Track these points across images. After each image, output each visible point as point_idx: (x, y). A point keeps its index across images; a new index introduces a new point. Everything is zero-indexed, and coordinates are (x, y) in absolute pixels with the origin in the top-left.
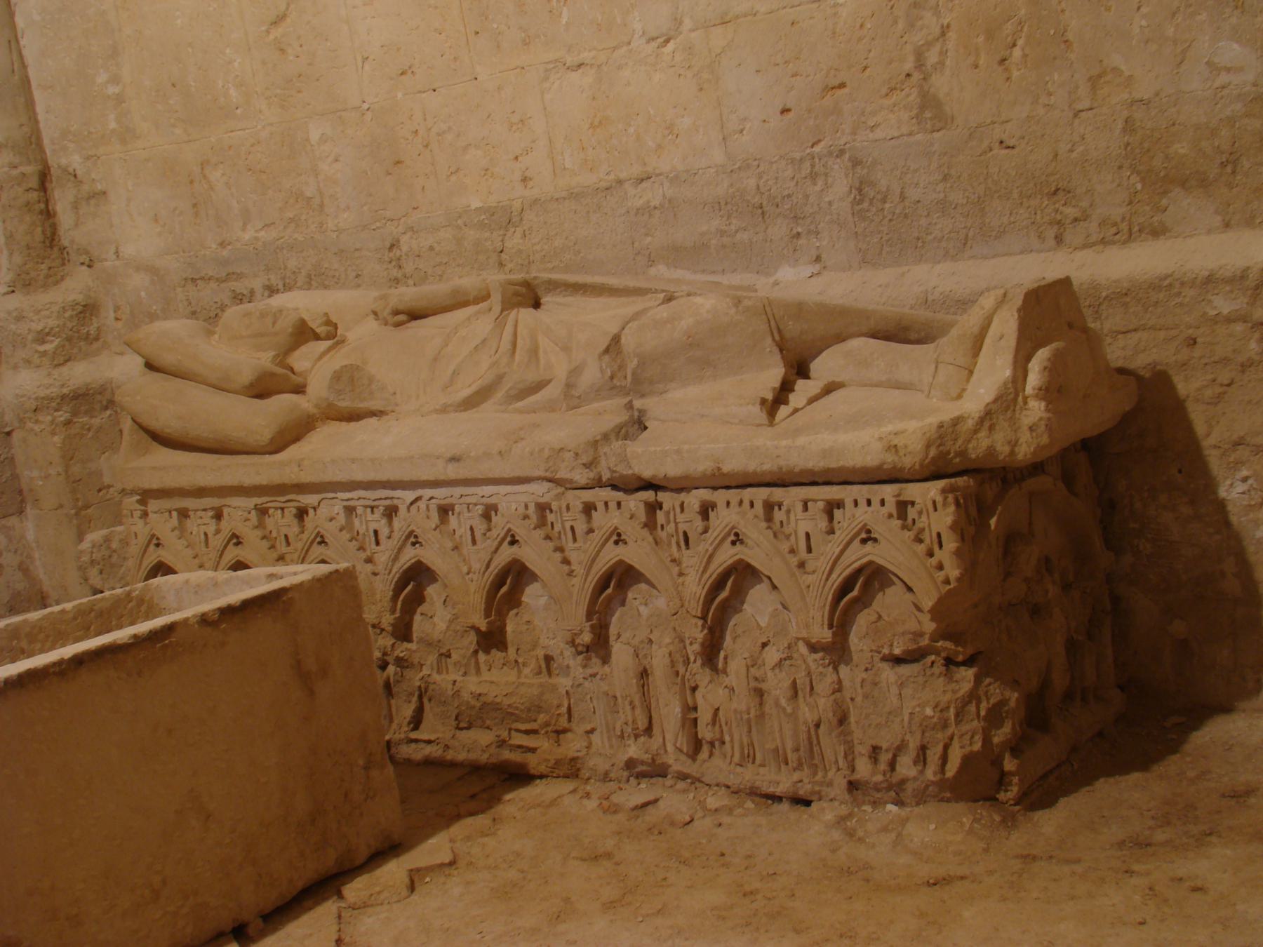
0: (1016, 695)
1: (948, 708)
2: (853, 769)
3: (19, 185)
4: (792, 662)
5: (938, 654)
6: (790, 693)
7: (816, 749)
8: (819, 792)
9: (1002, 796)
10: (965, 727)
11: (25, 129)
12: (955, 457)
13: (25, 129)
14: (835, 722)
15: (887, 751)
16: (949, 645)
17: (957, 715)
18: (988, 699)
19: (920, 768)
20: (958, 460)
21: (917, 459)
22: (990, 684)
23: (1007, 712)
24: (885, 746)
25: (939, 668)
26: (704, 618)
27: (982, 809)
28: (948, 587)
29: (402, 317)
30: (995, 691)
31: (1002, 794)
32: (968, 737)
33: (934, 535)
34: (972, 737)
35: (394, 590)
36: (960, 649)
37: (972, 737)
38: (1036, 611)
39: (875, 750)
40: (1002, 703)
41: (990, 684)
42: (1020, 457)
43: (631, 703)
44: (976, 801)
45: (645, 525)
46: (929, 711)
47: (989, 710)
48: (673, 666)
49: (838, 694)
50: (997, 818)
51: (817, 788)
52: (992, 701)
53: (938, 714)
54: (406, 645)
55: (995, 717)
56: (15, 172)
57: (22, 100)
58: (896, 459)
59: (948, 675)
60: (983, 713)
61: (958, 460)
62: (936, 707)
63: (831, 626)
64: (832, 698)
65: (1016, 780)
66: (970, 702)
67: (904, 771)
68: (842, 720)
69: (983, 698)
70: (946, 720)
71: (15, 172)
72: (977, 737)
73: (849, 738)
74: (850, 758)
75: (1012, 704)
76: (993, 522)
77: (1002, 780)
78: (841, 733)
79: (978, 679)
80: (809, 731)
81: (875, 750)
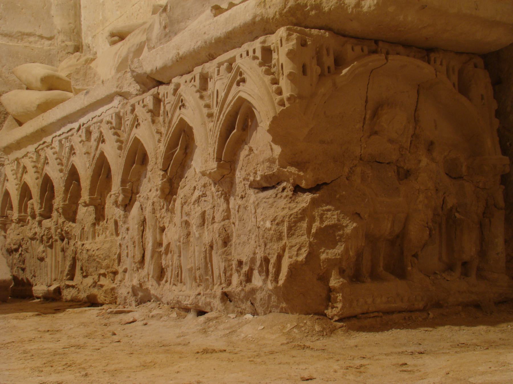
0: (355, 225)
1: (283, 221)
2: (229, 284)
3: (64, 50)
4: (206, 198)
5: (288, 181)
6: (199, 221)
7: (209, 265)
8: (209, 304)
9: (329, 312)
10: (294, 240)
11: (71, 25)
12: (312, 10)
13: (71, 25)
14: (220, 243)
15: (246, 264)
16: (293, 170)
17: (290, 228)
18: (322, 221)
19: (263, 277)
20: (313, 12)
21: (277, 9)
22: (329, 210)
23: (341, 236)
24: (244, 260)
25: (289, 192)
26: (166, 171)
27: (308, 321)
28: (282, 108)
29: (116, 38)
30: (332, 217)
31: (330, 310)
32: (295, 249)
33: (280, 65)
34: (299, 249)
35: (65, 186)
36: (302, 174)
37: (299, 249)
38: (405, 175)
39: (240, 263)
40: (336, 227)
41: (329, 210)
42: (365, 9)
43: (134, 242)
44: (308, 314)
45: (150, 111)
46: (268, 225)
47: (320, 230)
48: (154, 213)
49: (227, 221)
50: (317, 328)
51: (208, 300)
52: (325, 224)
53: (274, 227)
54: (71, 223)
55: (327, 236)
56: (63, 44)
57: (73, 12)
58: (263, 11)
59: (292, 199)
60: (314, 231)
61: (313, 12)
62: (274, 220)
63: (219, 159)
64: (223, 223)
65: (340, 297)
66: (302, 219)
67: (256, 283)
68: (226, 242)
69: (318, 219)
70: (281, 233)
71: (63, 44)
72: (303, 250)
73: (229, 257)
74: (228, 274)
75: (348, 230)
76: (344, 71)
77: (329, 299)
78: (223, 253)
79: (314, 203)
80: (206, 251)
81: (240, 263)
